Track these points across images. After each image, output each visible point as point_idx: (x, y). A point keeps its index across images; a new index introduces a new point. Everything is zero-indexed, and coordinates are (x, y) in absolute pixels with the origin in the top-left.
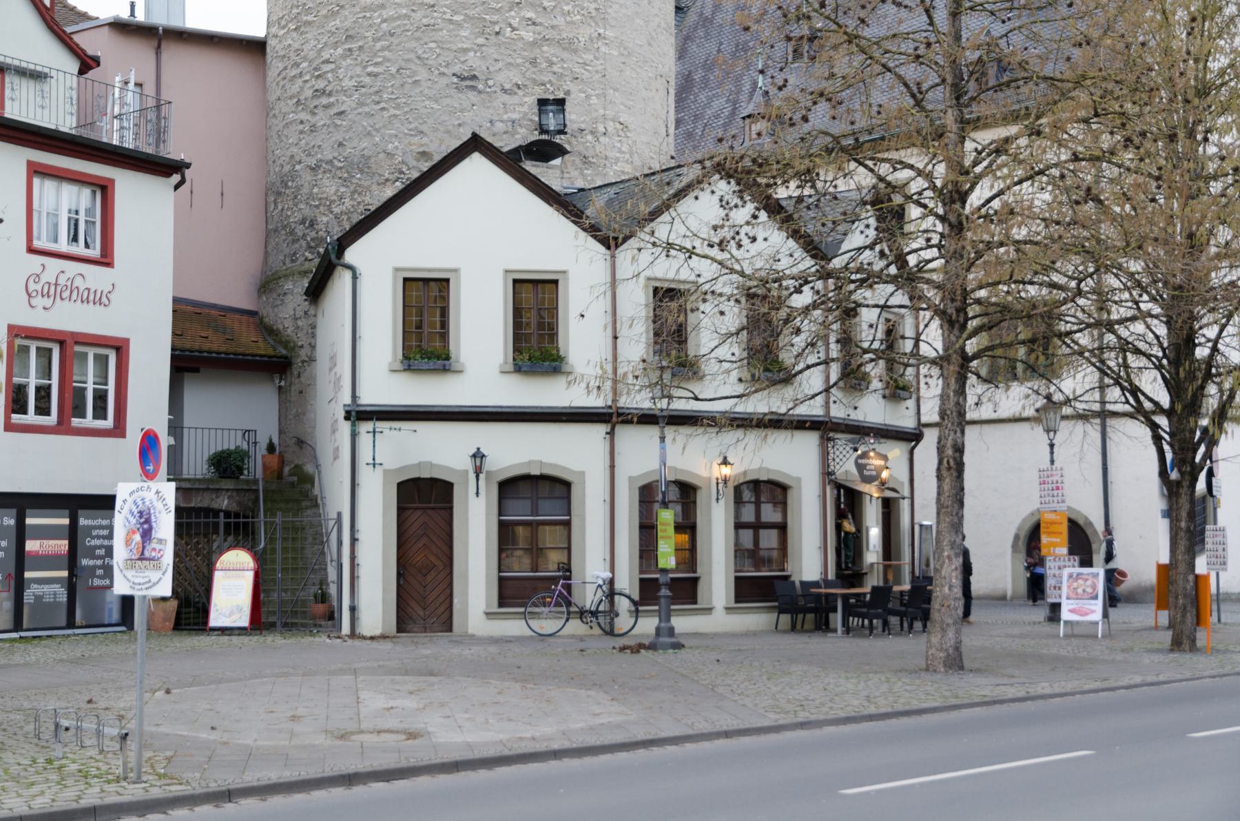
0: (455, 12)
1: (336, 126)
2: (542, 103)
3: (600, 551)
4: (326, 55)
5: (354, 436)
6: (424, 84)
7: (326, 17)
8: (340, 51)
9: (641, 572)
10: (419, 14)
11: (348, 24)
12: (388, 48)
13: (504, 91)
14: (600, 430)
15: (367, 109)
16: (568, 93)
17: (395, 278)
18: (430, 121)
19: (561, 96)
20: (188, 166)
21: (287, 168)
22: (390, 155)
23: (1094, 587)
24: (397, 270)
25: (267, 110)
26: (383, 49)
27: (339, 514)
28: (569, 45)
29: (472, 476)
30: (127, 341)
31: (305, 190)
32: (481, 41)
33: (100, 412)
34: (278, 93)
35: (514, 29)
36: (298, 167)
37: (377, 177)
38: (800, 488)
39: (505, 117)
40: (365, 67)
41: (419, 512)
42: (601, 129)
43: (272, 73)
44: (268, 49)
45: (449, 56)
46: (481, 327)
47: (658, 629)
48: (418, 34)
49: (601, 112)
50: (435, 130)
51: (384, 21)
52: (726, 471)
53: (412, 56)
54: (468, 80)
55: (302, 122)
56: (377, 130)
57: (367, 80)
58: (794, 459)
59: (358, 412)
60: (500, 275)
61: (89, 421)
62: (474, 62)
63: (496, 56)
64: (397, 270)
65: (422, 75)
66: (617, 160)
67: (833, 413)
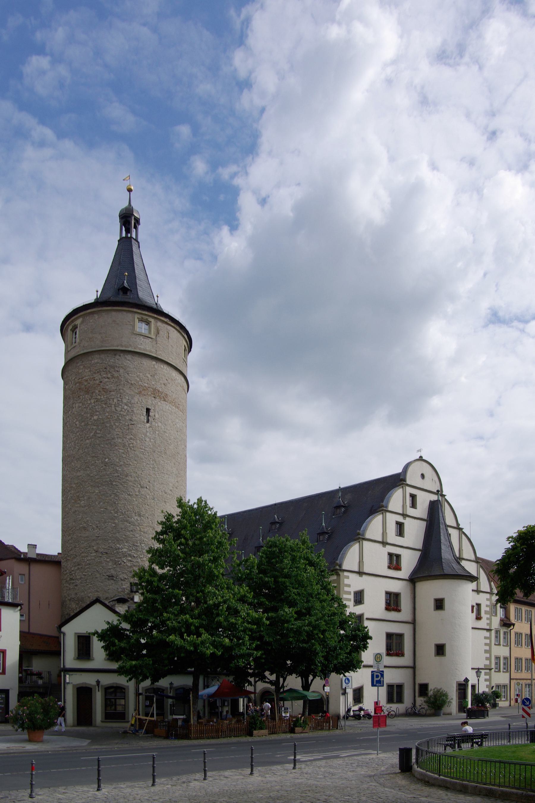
0: (107, 558)
12: (88, 568)
17: (75, 636)
22: (89, 597)
30: (5, 650)
32: (115, 566)
43: (63, 570)
54: (111, 577)
57: (83, 576)
62: (113, 572)
64: (76, 633)
65: (98, 575)
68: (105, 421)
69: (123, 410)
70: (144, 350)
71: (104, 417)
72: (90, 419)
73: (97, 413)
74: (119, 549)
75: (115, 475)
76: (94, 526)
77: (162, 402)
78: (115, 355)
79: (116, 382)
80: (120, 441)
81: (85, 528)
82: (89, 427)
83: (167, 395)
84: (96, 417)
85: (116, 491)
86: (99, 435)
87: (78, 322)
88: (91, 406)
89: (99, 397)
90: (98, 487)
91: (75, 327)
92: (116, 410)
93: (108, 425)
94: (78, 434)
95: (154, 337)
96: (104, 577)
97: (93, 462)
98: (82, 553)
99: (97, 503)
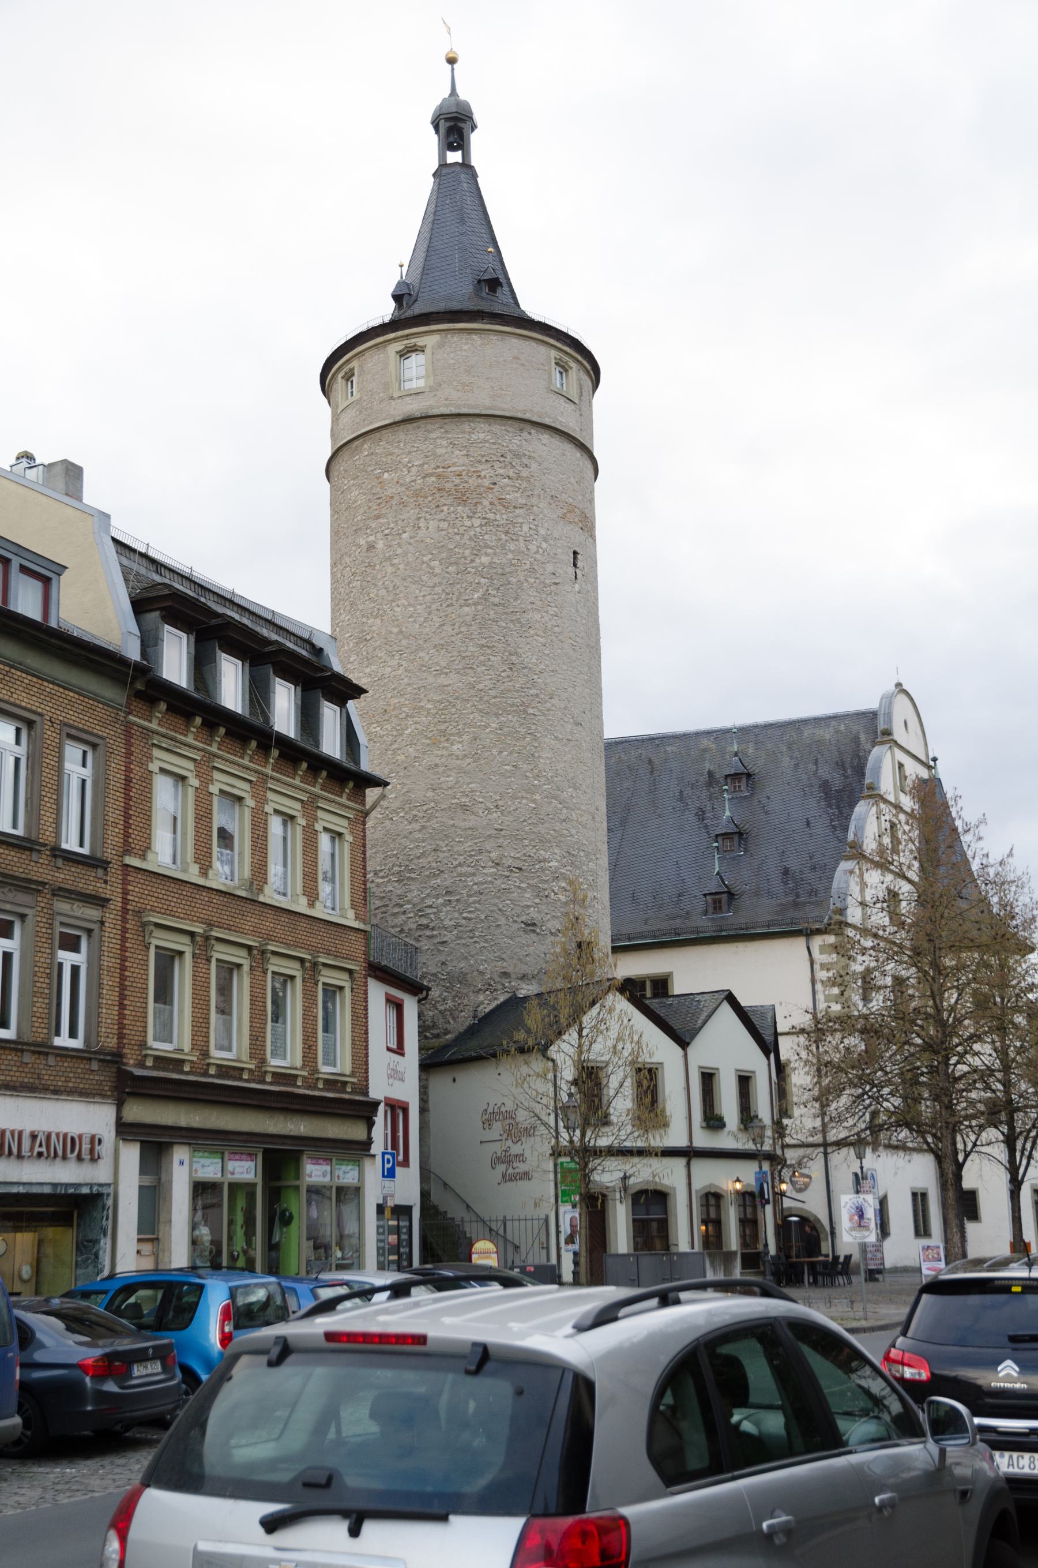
0: (522, 882)
1: (439, 950)
3: (685, 1234)
4: (429, 902)
6: (503, 927)
7: (428, 876)
8: (441, 901)
10: (499, 882)
11: (447, 883)
12: (479, 902)
13: (552, 934)
14: (681, 1162)
23: (938, 1254)
26: (475, 902)
32: (537, 901)
35: (556, 894)
40: (461, 913)
45: (519, 910)
48: (498, 895)
51: (475, 884)
52: (738, 1186)
53: (495, 908)
54: (531, 926)
57: (464, 922)
62: (534, 914)
65: (502, 921)
68: (508, 570)
69: (541, 551)
70: (490, 408)
71: (504, 561)
72: (472, 561)
73: (489, 551)
74: (544, 860)
75: (531, 692)
78: (521, 430)
79: (525, 489)
80: (537, 616)
81: (465, 808)
82: (469, 578)
84: (485, 560)
85: (533, 727)
86: (496, 600)
88: (472, 533)
89: (491, 516)
90: (497, 715)
93: (513, 580)
96: (516, 926)
97: (482, 658)
98: (460, 865)
99: (494, 751)
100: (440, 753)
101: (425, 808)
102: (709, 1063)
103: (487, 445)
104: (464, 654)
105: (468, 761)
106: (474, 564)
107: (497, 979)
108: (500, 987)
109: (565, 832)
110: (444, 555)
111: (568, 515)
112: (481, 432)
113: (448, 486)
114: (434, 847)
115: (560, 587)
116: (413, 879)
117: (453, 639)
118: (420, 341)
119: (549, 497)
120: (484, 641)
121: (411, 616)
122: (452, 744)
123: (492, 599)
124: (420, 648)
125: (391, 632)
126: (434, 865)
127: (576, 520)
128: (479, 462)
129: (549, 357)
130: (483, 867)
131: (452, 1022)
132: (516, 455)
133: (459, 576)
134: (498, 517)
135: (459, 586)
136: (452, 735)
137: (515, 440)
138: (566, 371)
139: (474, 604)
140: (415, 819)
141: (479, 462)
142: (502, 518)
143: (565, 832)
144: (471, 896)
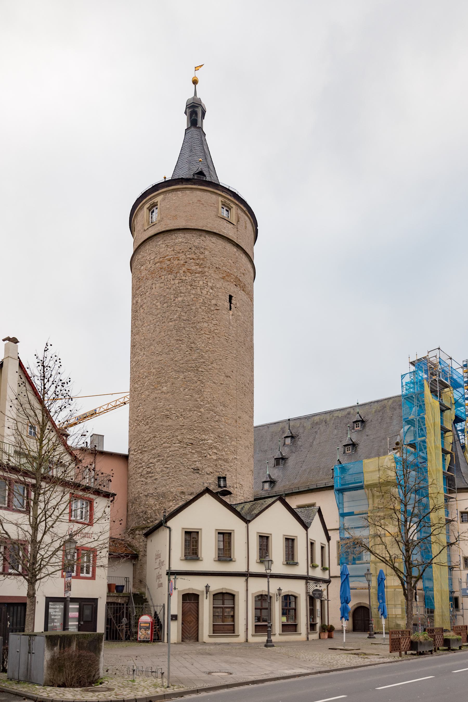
0: (193, 450)
1: (154, 483)
2: (219, 478)
4: (151, 461)
5: (169, 580)
7: (151, 449)
9: (255, 622)
10: (181, 450)
11: (158, 452)
12: (171, 460)
13: (207, 474)
14: (244, 579)
15: (164, 478)
16: (226, 475)
17: (182, 531)
18: (185, 482)
19: (224, 476)
20: (115, 495)
21: (137, 495)
22: (172, 493)
24: (183, 529)
25: (128, 477)
27: (164, 604)
28: (226, 461)
29: (205, 592)
31: (143, 502)
32: (200, 458)
33: (88, 572)
34: (134, 472)
36: (140, 495)
37: (167, 499)
38: (238, 595)
39: (207, 482)
40: (164, 465)
41: (188, 604)
42: (235, 486)
44: (129, 458)
46: (208, 546)
47: (267, 640)
49: (235, 481)
50: (186, 485)
53: (179, 462)
54: (196, 470)
55: (142, 481)
56: (168, 485)
57: (165, 469)
58: (298, 589)
59: (171, 573)
60: (214, 531)
61: (84, 575)
62: (198, 465)
63: (205, 463)
66: (240, 496)
67: (309, 575)
69: (209, 294)
72: (174, 300)
73: (182, 294)
74: (205, 440)
75: (201, 360)
76: (178, 414)
77: (242, 292)
78: (201, 236)
80: (206, 325)
81: (167, 417)
83: (245, 285)
84: (180, 299)
85: (201, 377)
86: (185, 318)
87: (159, 199)
88: (174, 287)
89: (184, 278)
90: (183, 372)
91: (154, 205)
92: (202, 293)
93: (194, 308)
94: (159, 316)
95: (235, 224)
96: (189, 470)
98: (164, 443)
99: (181, 389)
100: (157, 392)
101: (151, 418)
102: (265, 531)
103: (183, 244)
104: (169, 345)
105: (169, 394)
106: (175, 302)
107: (179, 495)
108: (180, 498)
109: (217, 427)
110: (162, 299)
111: (226, 277)
112: (180, 238)
113: (165, 266)
114: (154, 435)
115: (220, 311)
116: (146, 451)
117: (165, 338)
118: (155, 200)
119: (214, 268)
120: (178, 338)
121: (149, 330)
122: (163, 387)
123: (183, 317)
124: (151, 344)
125: (141, 340)
126: (153, 444)
127: (232, 280)
128: (179, 253)
129: (218, 200)
130: (174, 443)
131: (158, 514)
132: (197, 248)
133: (168, 308)
134: (187, 278)
135: (168, 313)
136: (163, 383)
137: (196, 240)
138: (230, 209)
139: (174, 320)
140: (147, 424)
141: (179, 253)
142: (189, 278)
143: (217, 427)
144: (169, 457)
